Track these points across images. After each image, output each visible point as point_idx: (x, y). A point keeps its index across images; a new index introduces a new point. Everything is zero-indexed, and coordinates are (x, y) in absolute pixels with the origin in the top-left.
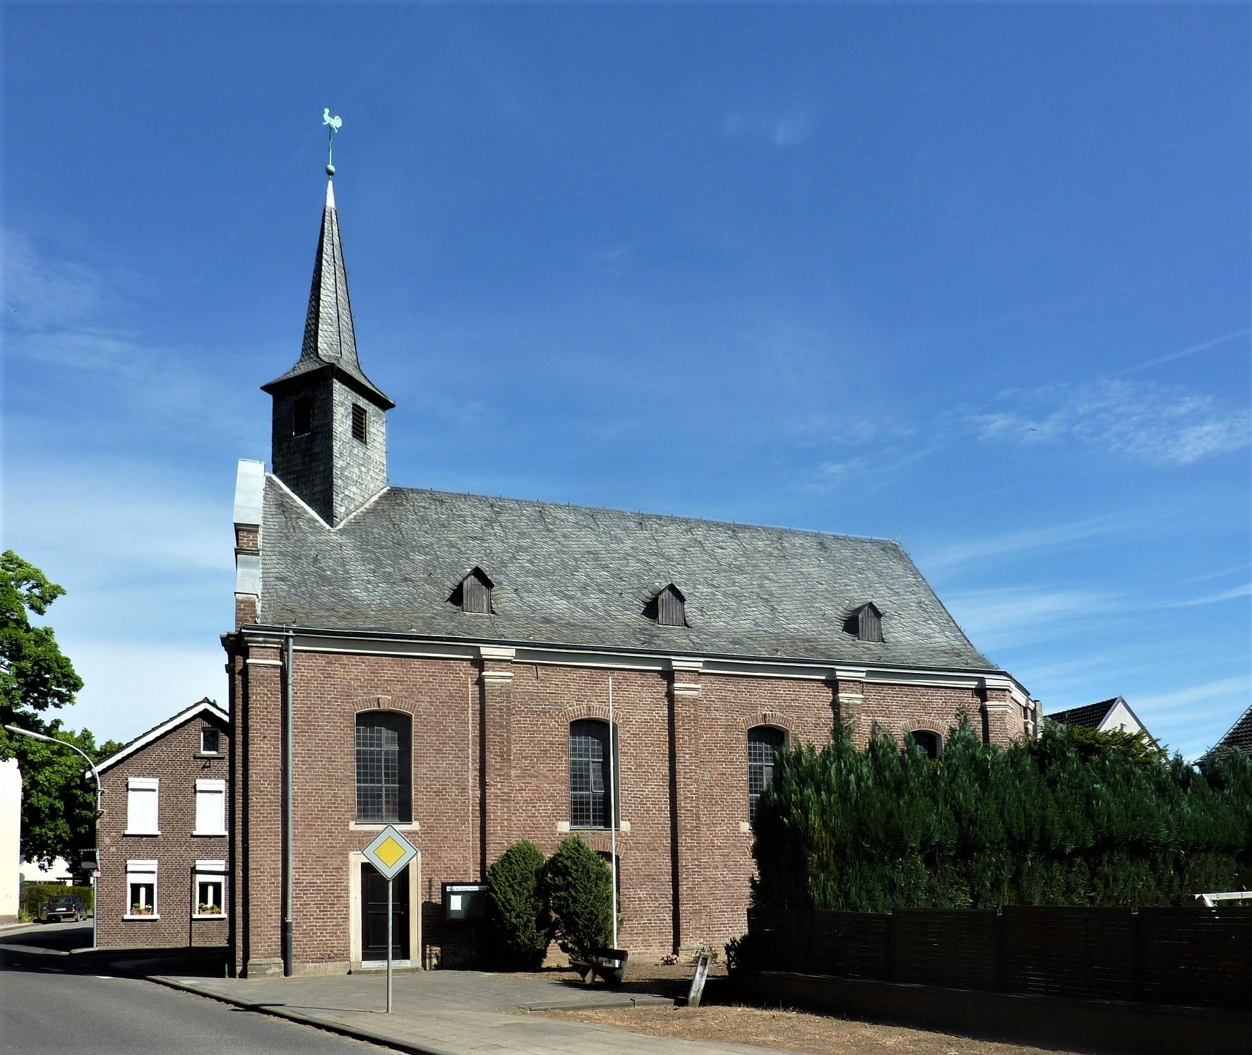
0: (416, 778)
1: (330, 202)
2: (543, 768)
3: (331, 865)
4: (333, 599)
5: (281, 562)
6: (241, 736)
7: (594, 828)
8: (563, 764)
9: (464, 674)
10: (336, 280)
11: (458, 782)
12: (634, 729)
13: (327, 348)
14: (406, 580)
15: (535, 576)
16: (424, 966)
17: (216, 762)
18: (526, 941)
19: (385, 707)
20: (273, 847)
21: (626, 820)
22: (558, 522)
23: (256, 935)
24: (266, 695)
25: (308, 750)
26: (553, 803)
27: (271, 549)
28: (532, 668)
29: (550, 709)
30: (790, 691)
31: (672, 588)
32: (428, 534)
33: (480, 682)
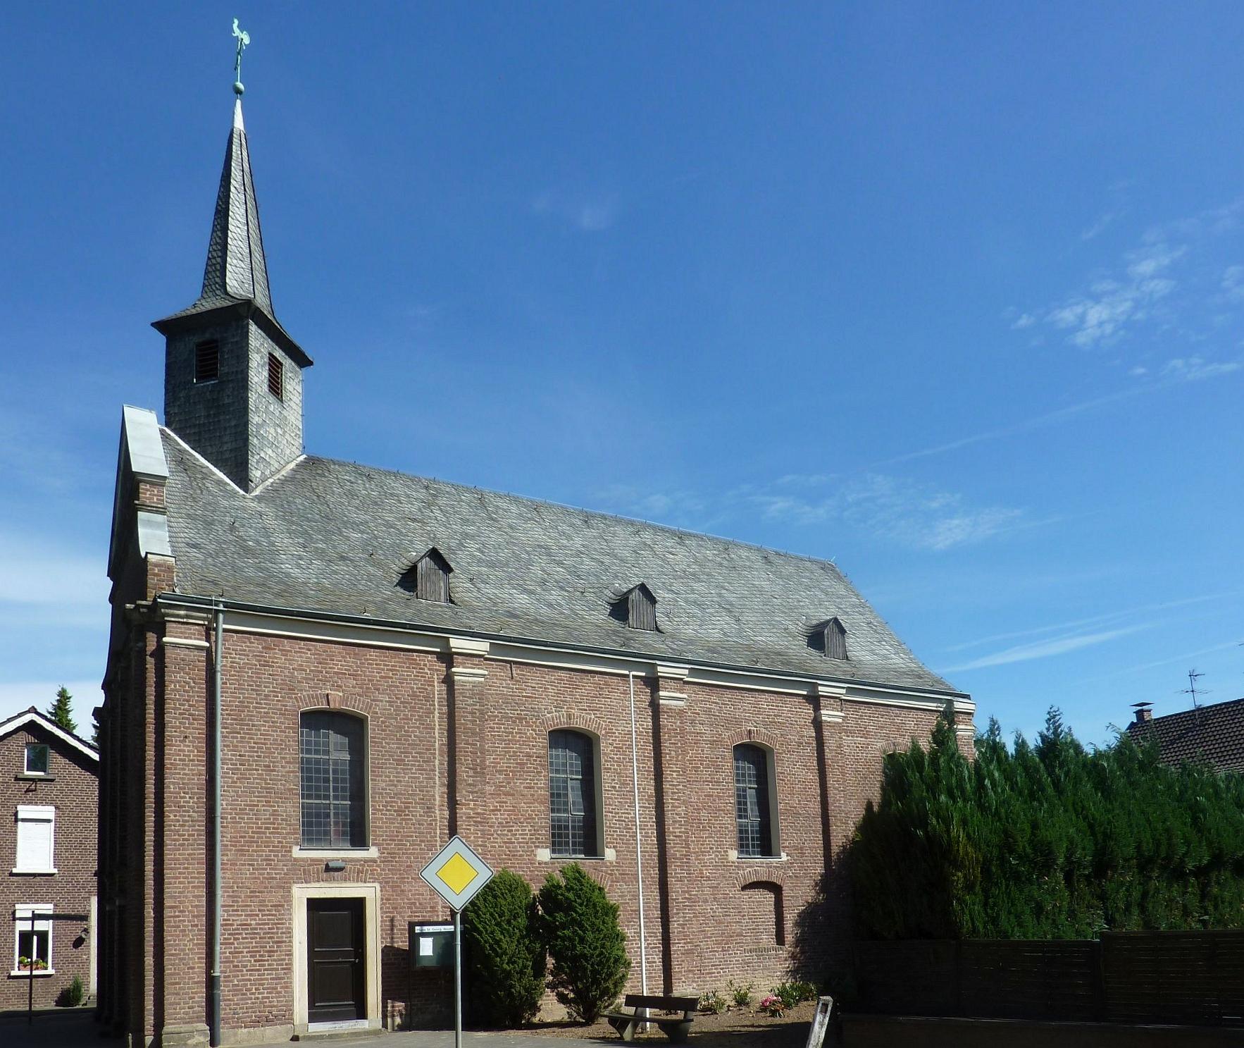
0: (373, 793)
1: (239, 123)
2: (520, 785)
3: (269, 901)
4: (261, 574)
5: (190, 526)
7: (574, 856)
8: (542, 780)
9: (429, 669)
10: (247, 210)
11: (423, 799)
12: (617, 742)
13: (237, 286)
14: (343, 558)
15: (488, 566)
16: (385, 1025)
17: (43, 785)
18: (523, 992)
19: (335, 705)
20: (195, 878)
21: (610, 848)
22: (501, 512)
23: (174, 994)
24: (188, 683)
25: (240, 755)
26: (531, 826)
27: (176, 510)
28: (506, 667)
29: (527, 715)
30: (773, 706)
31: (643, 588)
32: (359, 510)
33: (449, 681)
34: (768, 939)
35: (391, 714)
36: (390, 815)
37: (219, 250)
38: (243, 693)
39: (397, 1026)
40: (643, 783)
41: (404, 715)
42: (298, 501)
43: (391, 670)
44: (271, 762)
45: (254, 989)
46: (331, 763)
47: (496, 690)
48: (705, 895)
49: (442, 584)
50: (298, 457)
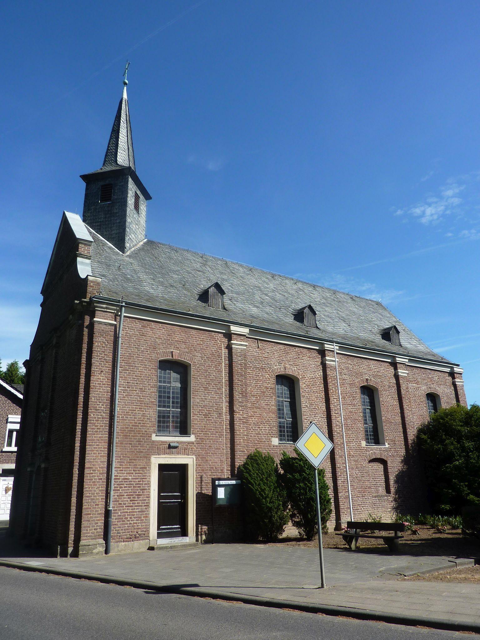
1: (125, 96)
3: (139, 465)
5: (100, 266)
6: (85, 370)
7: (288, 443)
8: (273, 401)
9: (220, 341)
11: (217, 409)
12: (307, 382)
13: (122, 161)
14: (172, 286)
16: (197, 540)
20: (102, 451)
26: (269, 425)
28: (255, 342)
30: (376, 367)
31: (310, 307)
33: (229, 348)
34: (382, 490)
35: (202, 364)
36: (201, 417)
37: (114, 146)
38: (131, 349)
39: (204, 541)
40: (320, 404)
41: (208, 364)
42: (147, 259)
43: (202, 341)
44: (143, 386)
45: (129, 518)
46: (171, 388)
47: (251, 353)
48: (352, 465)
49: (220, 300)
50: (143, 240)
